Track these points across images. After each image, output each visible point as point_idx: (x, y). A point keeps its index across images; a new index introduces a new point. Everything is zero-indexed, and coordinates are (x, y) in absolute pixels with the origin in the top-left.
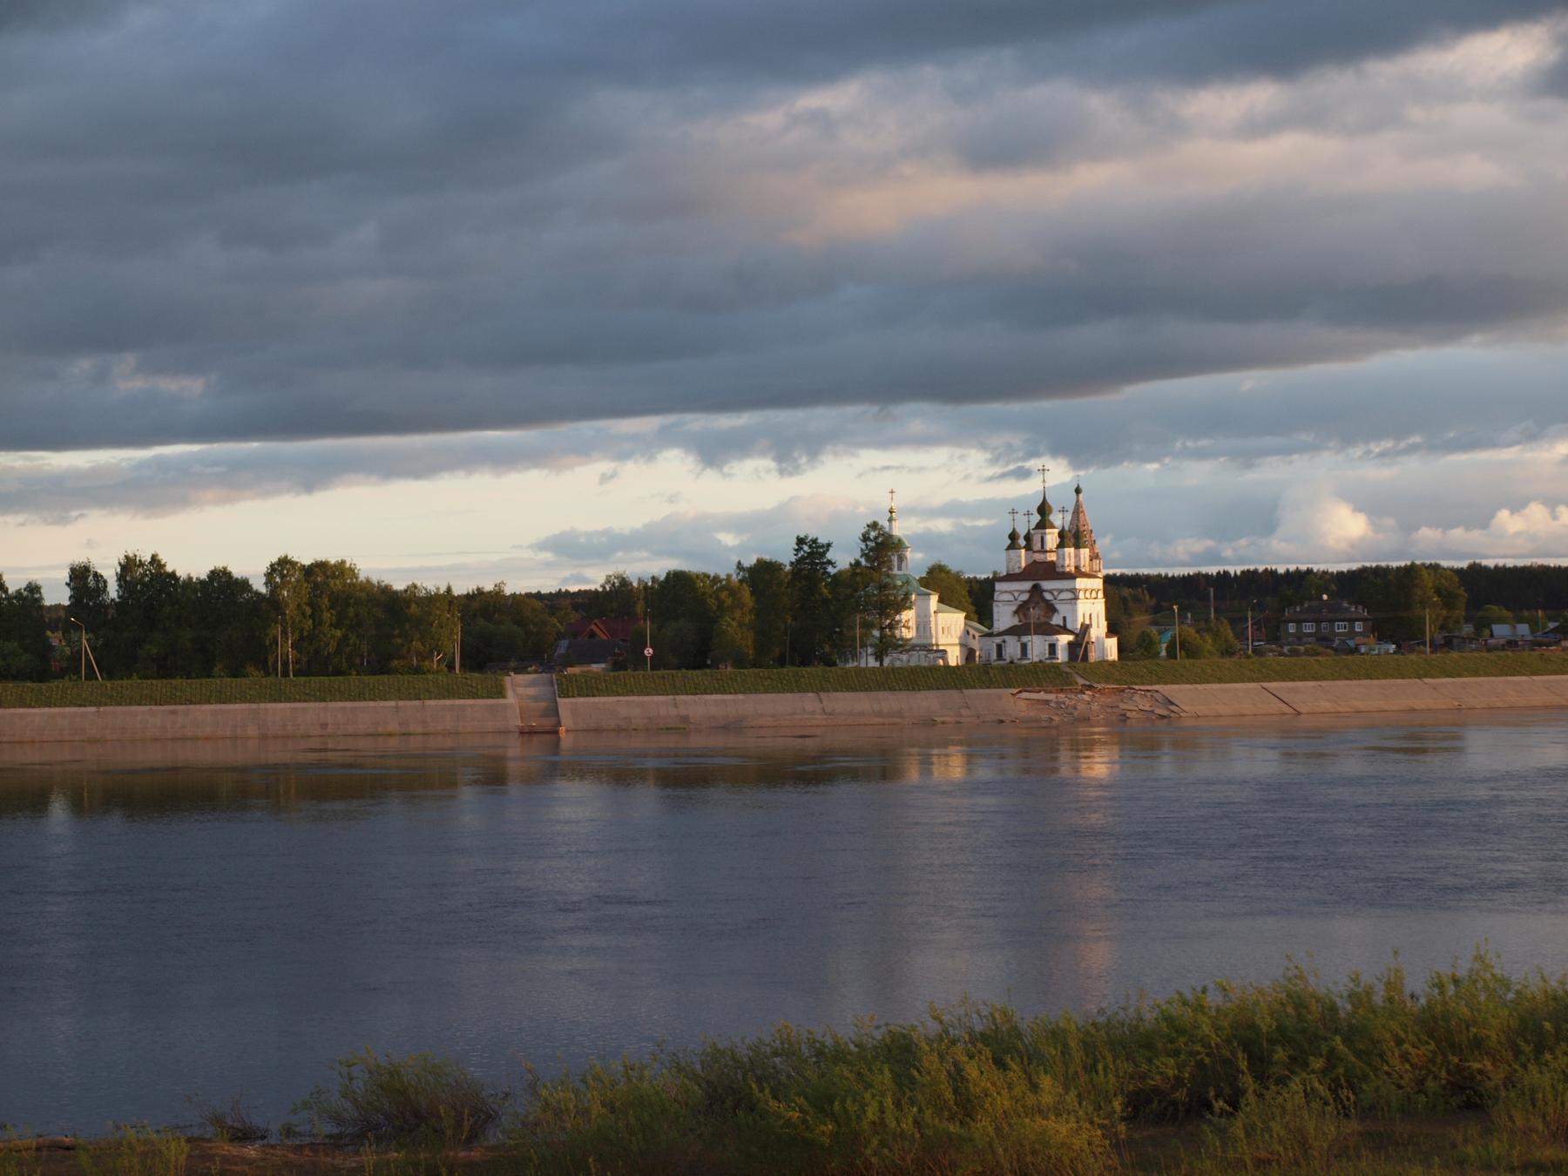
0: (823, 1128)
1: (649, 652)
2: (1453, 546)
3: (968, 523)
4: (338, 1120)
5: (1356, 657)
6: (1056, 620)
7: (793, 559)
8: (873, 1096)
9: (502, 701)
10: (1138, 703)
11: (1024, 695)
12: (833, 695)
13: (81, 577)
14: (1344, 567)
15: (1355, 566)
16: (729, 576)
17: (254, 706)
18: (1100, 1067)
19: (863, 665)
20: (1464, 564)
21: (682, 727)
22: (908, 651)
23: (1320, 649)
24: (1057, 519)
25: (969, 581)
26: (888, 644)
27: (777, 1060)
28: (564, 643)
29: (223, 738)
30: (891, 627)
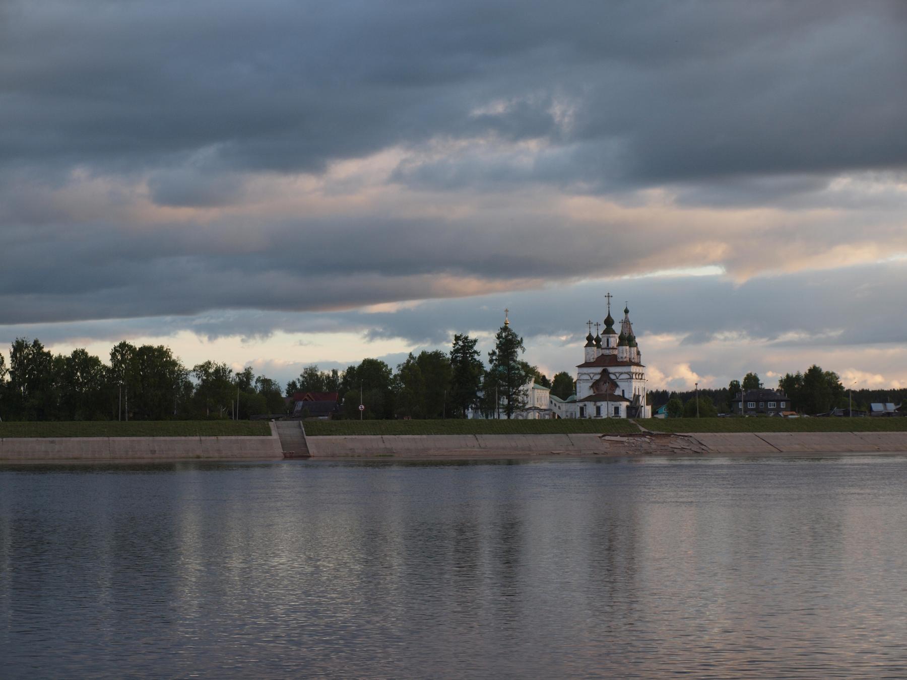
1: (362, 407)
6: (618, 392)
9: (269, 437)
11: (607, 438)
12: (485, 436)
24: (617, 327)
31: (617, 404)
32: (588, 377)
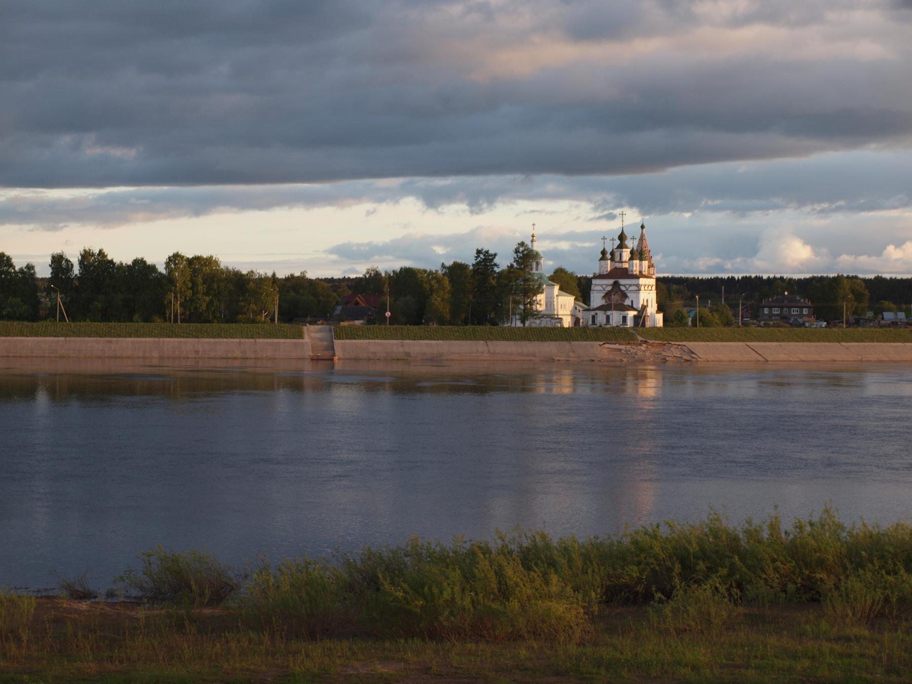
0: (417, 602)
1: (388, 314)
2: (867, 267)
3: (579, 244)
4: (142, 588)
5: (803, 329)
6: (627, 302)
7: (474, 262)
8: (449, 585)
9: (301, 341)
10: (673, 352)
11: (606, 346)
12: (495, 342)
13: (58, 262)
14: (802, 276)
15: (808, 276)
16: (437, 271)
17: (157, 339)
18: (589, 571)
19: (513, 325)
20: (872, 276)
21: (406, 359)
22: (539, 318)
23: (782, 324)
24: (631, 244)
25: (579, 279)
26: (528, 314)
27: (406, 559)
28: (339, 308)
29: (139, 358)
30: (531, 303)
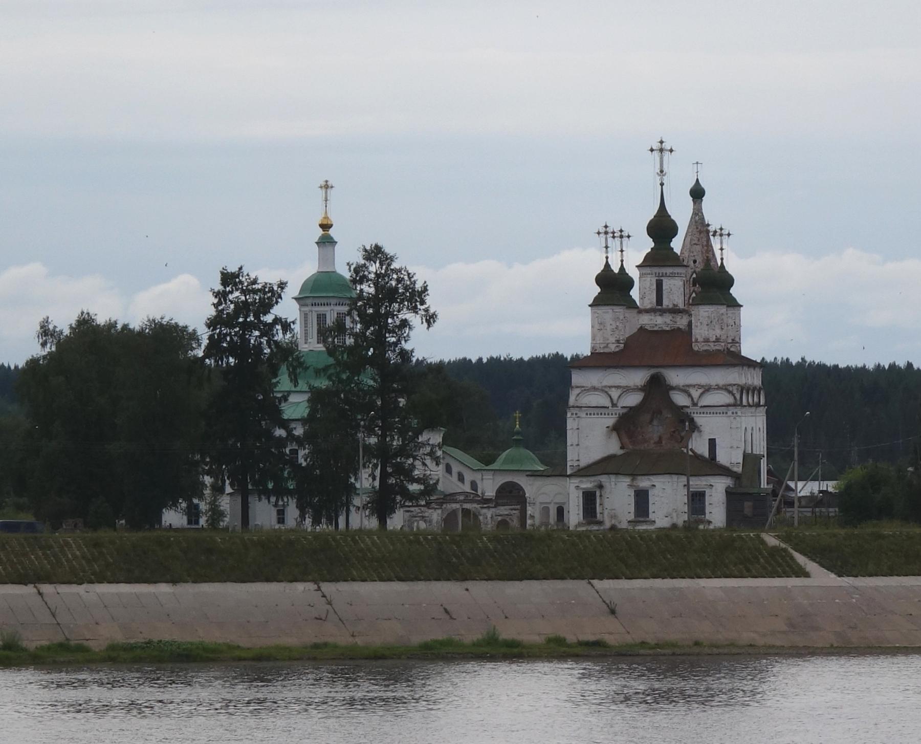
6: (699, 445)
31: (698, 483)
32: (603, 400)
